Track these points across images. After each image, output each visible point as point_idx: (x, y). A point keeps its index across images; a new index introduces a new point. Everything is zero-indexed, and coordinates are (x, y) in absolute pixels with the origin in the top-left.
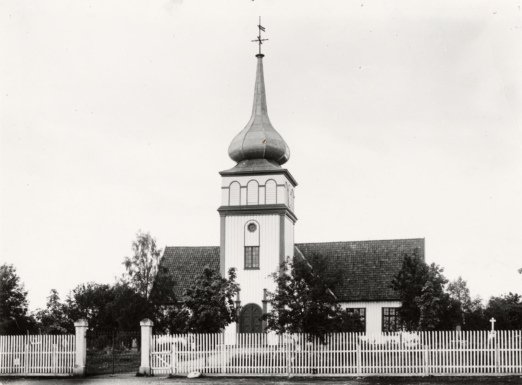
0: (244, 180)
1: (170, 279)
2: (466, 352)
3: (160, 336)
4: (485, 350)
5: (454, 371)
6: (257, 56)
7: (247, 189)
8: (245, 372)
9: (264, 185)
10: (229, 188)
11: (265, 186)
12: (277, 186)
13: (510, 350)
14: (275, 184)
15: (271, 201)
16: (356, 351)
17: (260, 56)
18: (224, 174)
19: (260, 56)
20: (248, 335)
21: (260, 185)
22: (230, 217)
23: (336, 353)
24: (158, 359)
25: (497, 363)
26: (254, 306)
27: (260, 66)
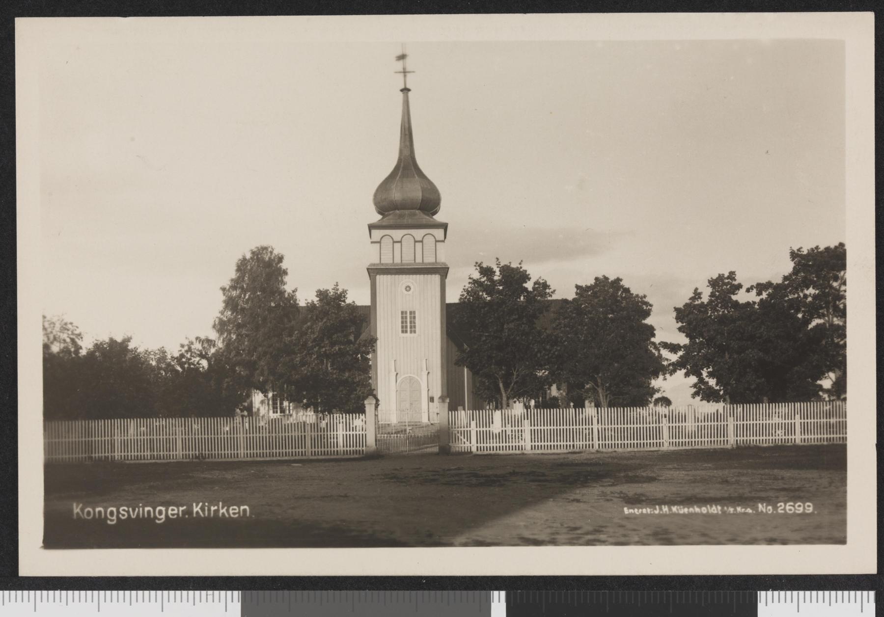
0: (397, 234)
1: (136, 351)
2: (634, 424)
3: (361, 415)
4: (816, 420)
5: (255, 455)
6: (402, 90)
7: (401, 245)
8: (484, 450)
9: (379, 240)
10: (380, 242)
11: (400, 242)
12: (436, 241)
13: (562, 427)
14: (434, 240)
15: (429, 259)
16: (800, 421)
17: (405, 90)
18: (371, 227)
19: (405, 90)
20: (804, 404)
21: (437, 239)
22: (382, 276)
23: (570, 429)
24: (464, 438)
25: (179, 450)
26: (411, 378)
27: (406, 104)
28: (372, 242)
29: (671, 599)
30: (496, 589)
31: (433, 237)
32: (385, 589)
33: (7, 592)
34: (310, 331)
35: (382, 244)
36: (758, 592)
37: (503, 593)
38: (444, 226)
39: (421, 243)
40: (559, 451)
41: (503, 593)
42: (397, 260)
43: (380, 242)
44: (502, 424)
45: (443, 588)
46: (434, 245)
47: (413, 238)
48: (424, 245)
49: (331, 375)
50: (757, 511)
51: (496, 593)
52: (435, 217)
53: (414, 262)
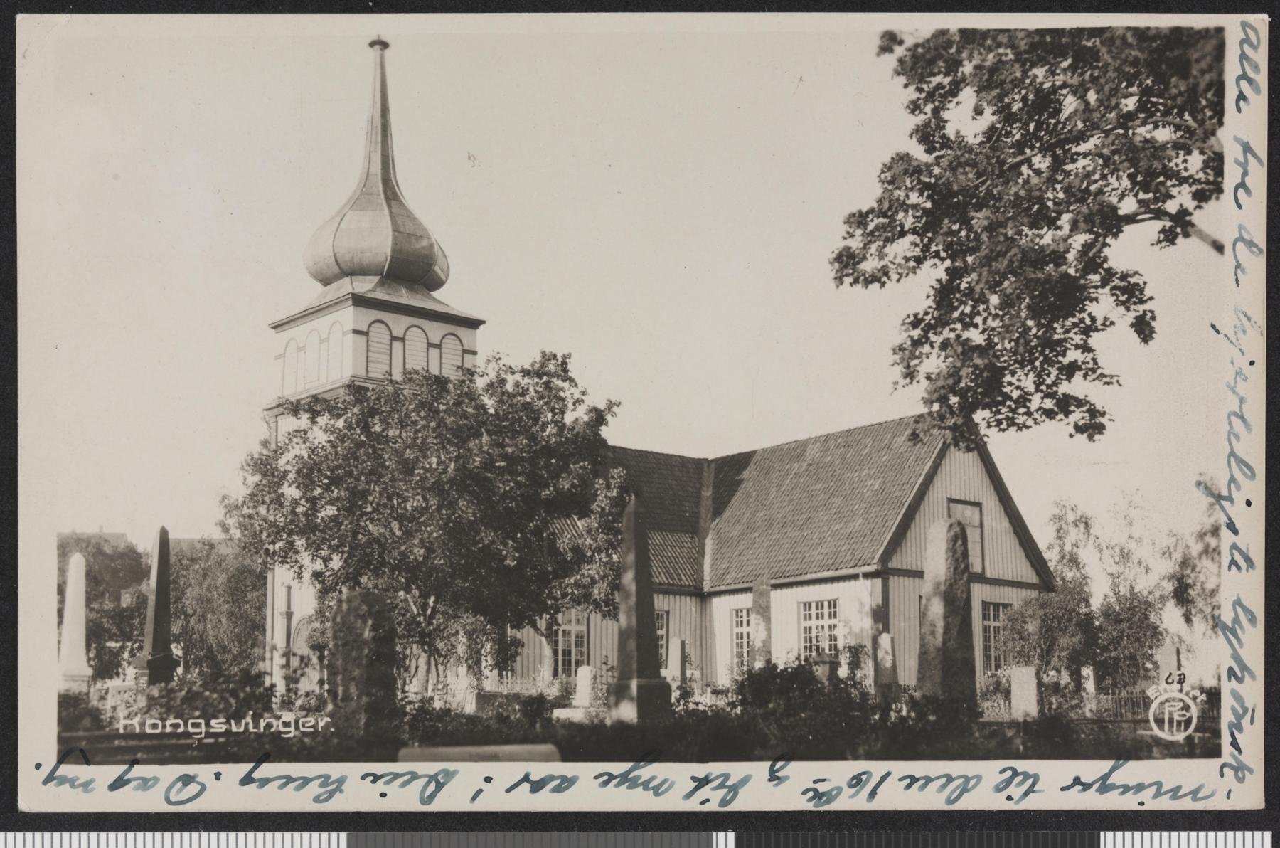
11: (439, 346)
29: (1022, 840)
30: (717, 830)
31: (458, 343)
32: (483, 830)
33: (10, 835)
35: (443, 350)
36: (1102, 834)
37: (731, 835)
41: (731, 835)
43: (366, 334)
44: (61, 591)
45: (567, 828)
47: (388, 332)
48: (407, 347)
51: (722, 835)
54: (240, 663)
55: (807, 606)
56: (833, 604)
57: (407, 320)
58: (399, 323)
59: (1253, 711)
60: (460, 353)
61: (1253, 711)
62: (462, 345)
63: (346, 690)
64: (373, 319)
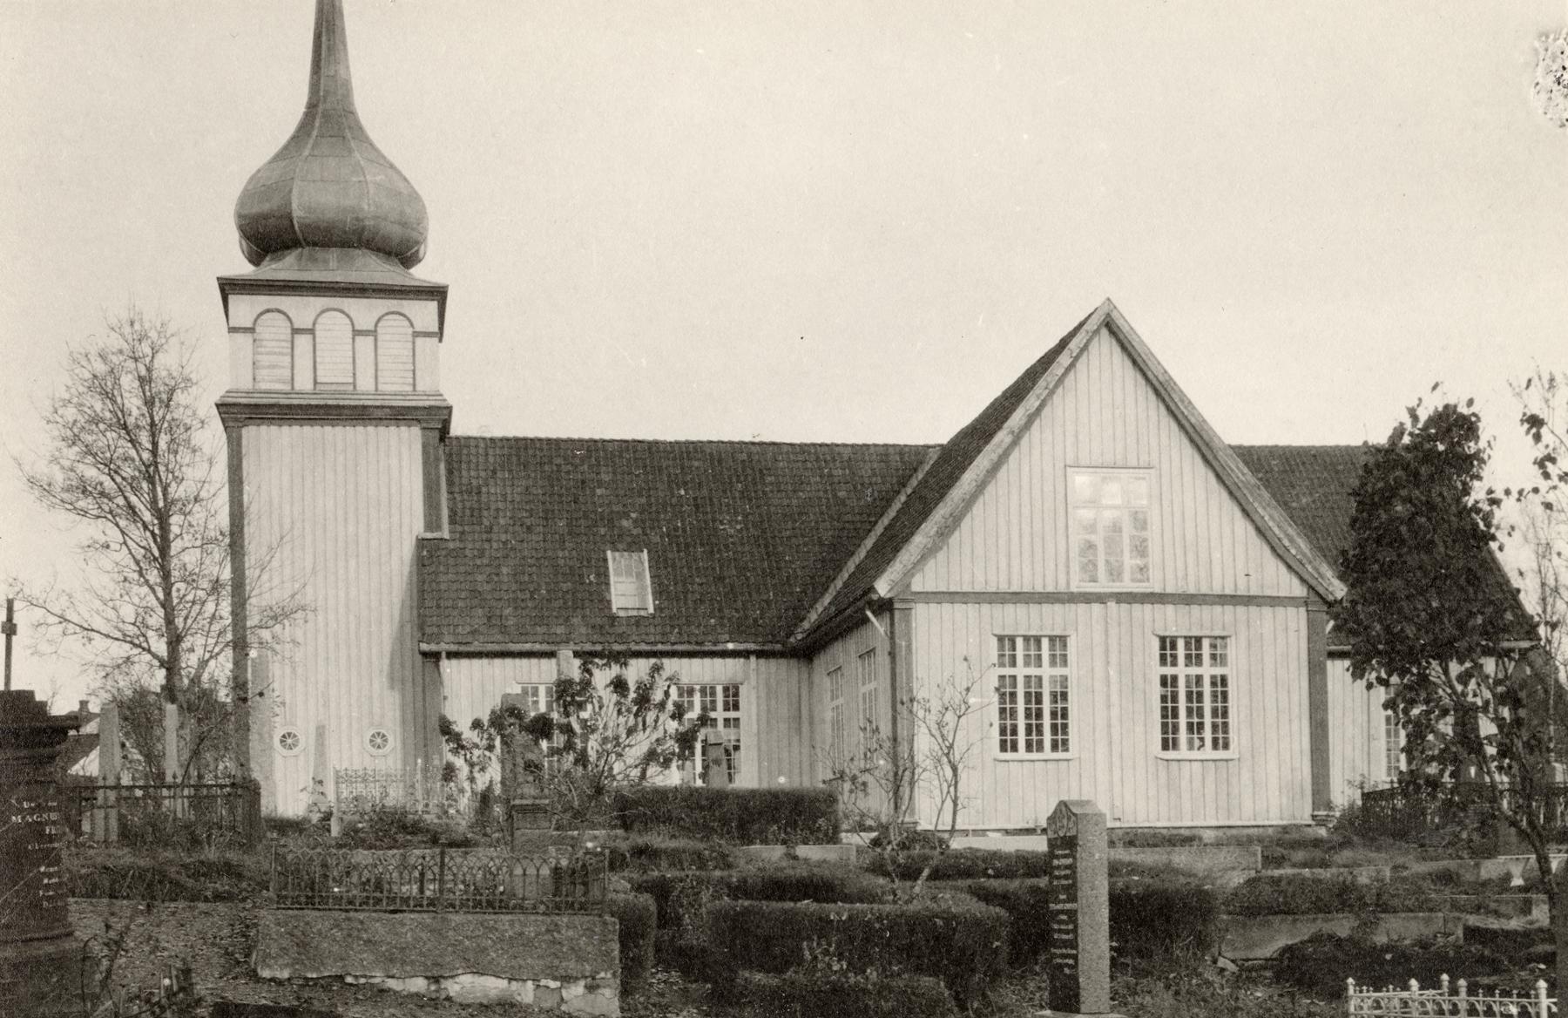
7: (376, 340)
11: (373, 333)
14: (350, 327)
21: (358, 327)
28: (232, 330)
31: (407, 323)
34: (1411, 788)
38: (438, 294)
39: (309, 337)
40: (525, 802)
42: (304, 383)
46: (410, 345)
48: (318, 340)
49: (1296, 961)
50: (96, 715)
52: (413, 271)
53: (409, 388)
54: (605, 740)
55: (1006, 641)
56: (1059, 641)
57: (381, 305)
58: (302, 309)
59: (321, 732)
60: (410, 338)
61: (321, 732)
62: (412, 325)
63: (1491, 778)
64: (266, 307)
